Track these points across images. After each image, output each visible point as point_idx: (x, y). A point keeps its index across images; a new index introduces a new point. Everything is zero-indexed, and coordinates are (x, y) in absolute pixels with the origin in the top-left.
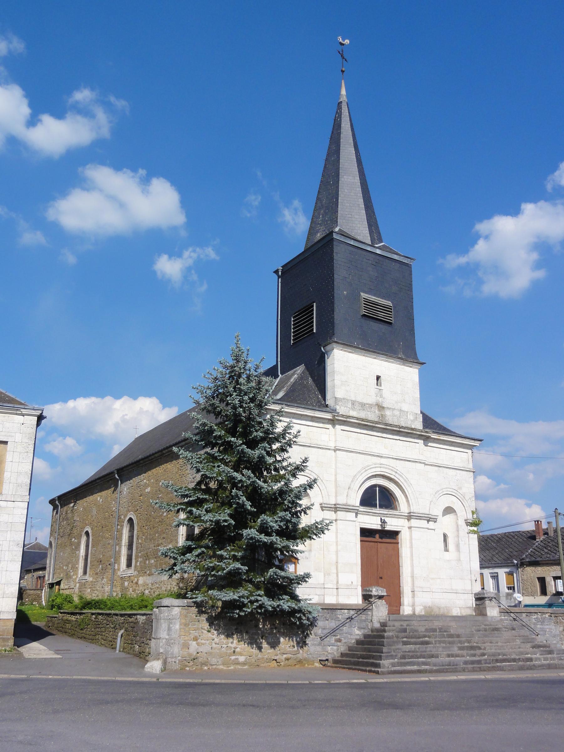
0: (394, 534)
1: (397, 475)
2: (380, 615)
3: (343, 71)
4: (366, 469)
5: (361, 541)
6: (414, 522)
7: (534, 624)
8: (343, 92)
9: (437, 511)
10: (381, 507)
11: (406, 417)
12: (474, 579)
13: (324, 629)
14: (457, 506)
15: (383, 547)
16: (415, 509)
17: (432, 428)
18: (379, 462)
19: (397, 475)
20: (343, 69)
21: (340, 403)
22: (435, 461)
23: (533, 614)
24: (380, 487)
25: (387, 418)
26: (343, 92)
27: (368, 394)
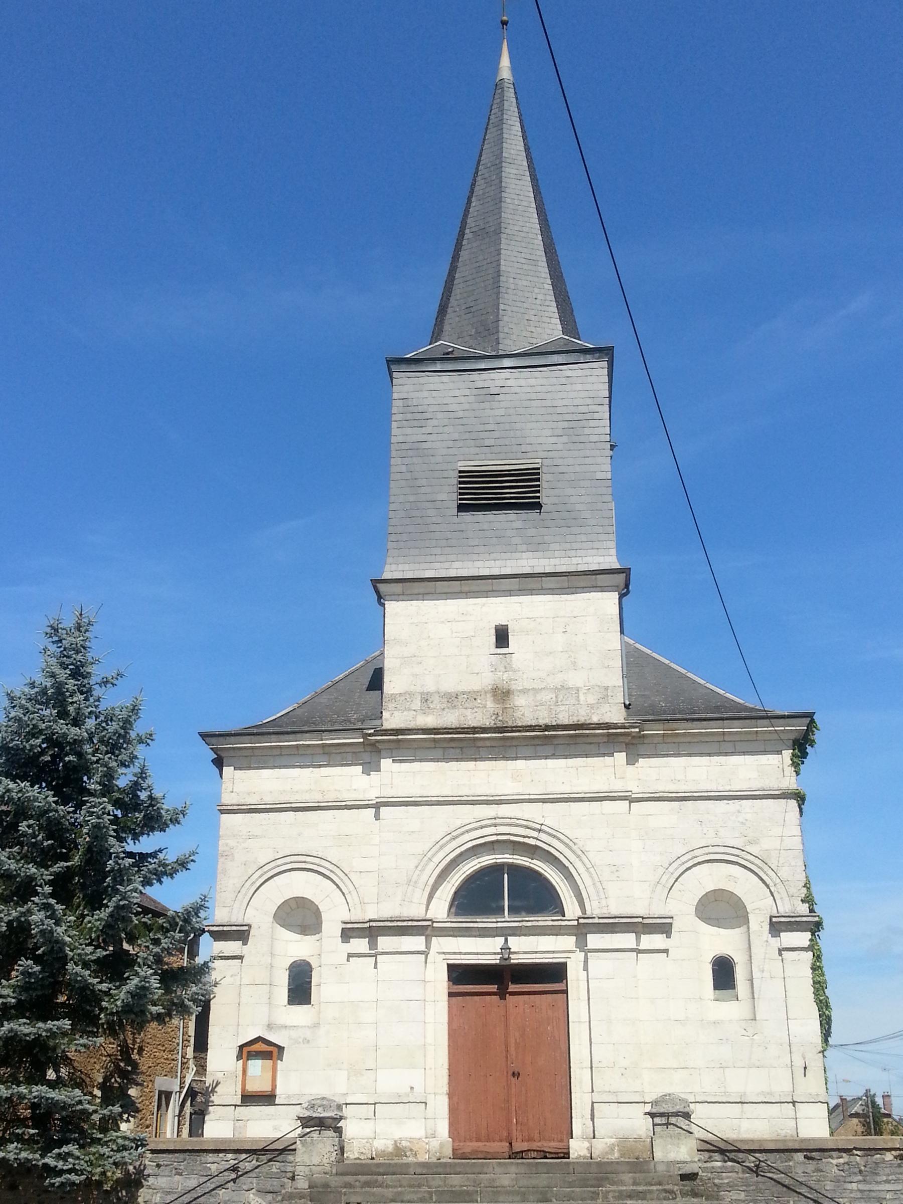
0: (552, 974)
1: (543, 836)
2: (316, 1160)
3: (504, 23)
4: (454, 834)
5: (451, 995)
6: (594, 941)
7: (836, 1180)
8: (505, 61)
9: (681, 907)
10: (513, 910)
11: (573, 701)
12: (799, 1063)
13: (169, 1193)
14: (742, 885)
15: (522, 1005)
16: (595, 909)
17: (664, 716)
18: (493, 815)
19: (543, 836)
20: (505, 18)
21: (391, 706)
22: (319, 797)
23: (834, 1154)
24: (514, 869)
25: (518, 714)
26: (505, 61)
27: (476, 668)
